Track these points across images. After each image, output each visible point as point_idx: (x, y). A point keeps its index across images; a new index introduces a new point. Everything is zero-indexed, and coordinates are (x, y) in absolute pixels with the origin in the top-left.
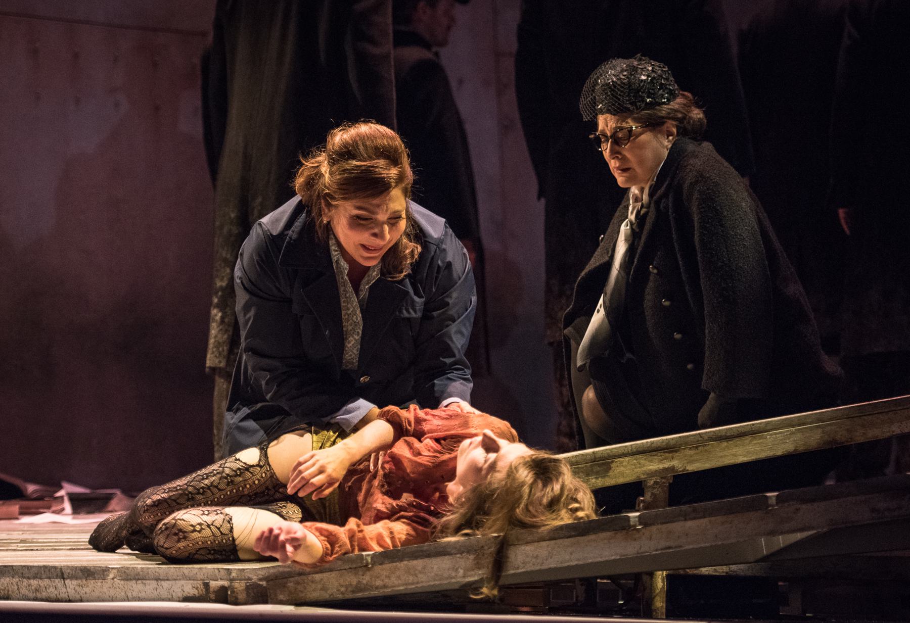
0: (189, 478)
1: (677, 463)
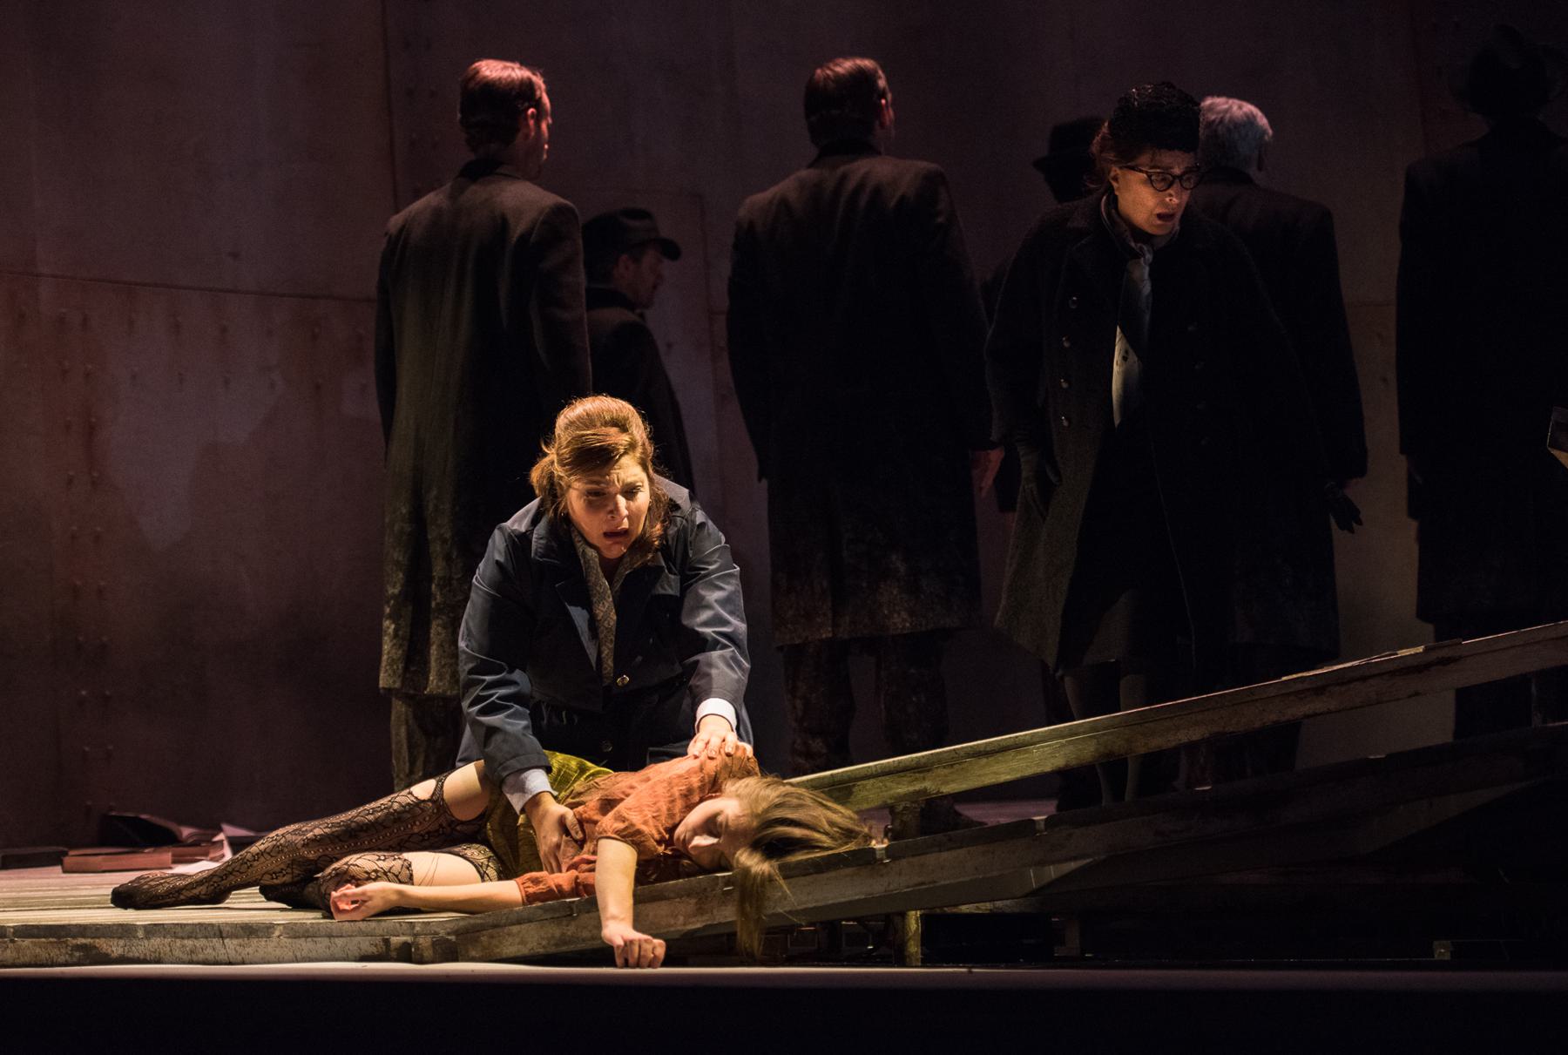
0: (354, 813)
1: (929, 784)
